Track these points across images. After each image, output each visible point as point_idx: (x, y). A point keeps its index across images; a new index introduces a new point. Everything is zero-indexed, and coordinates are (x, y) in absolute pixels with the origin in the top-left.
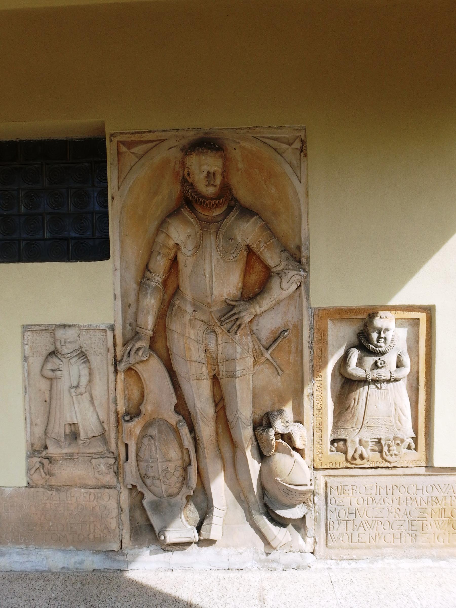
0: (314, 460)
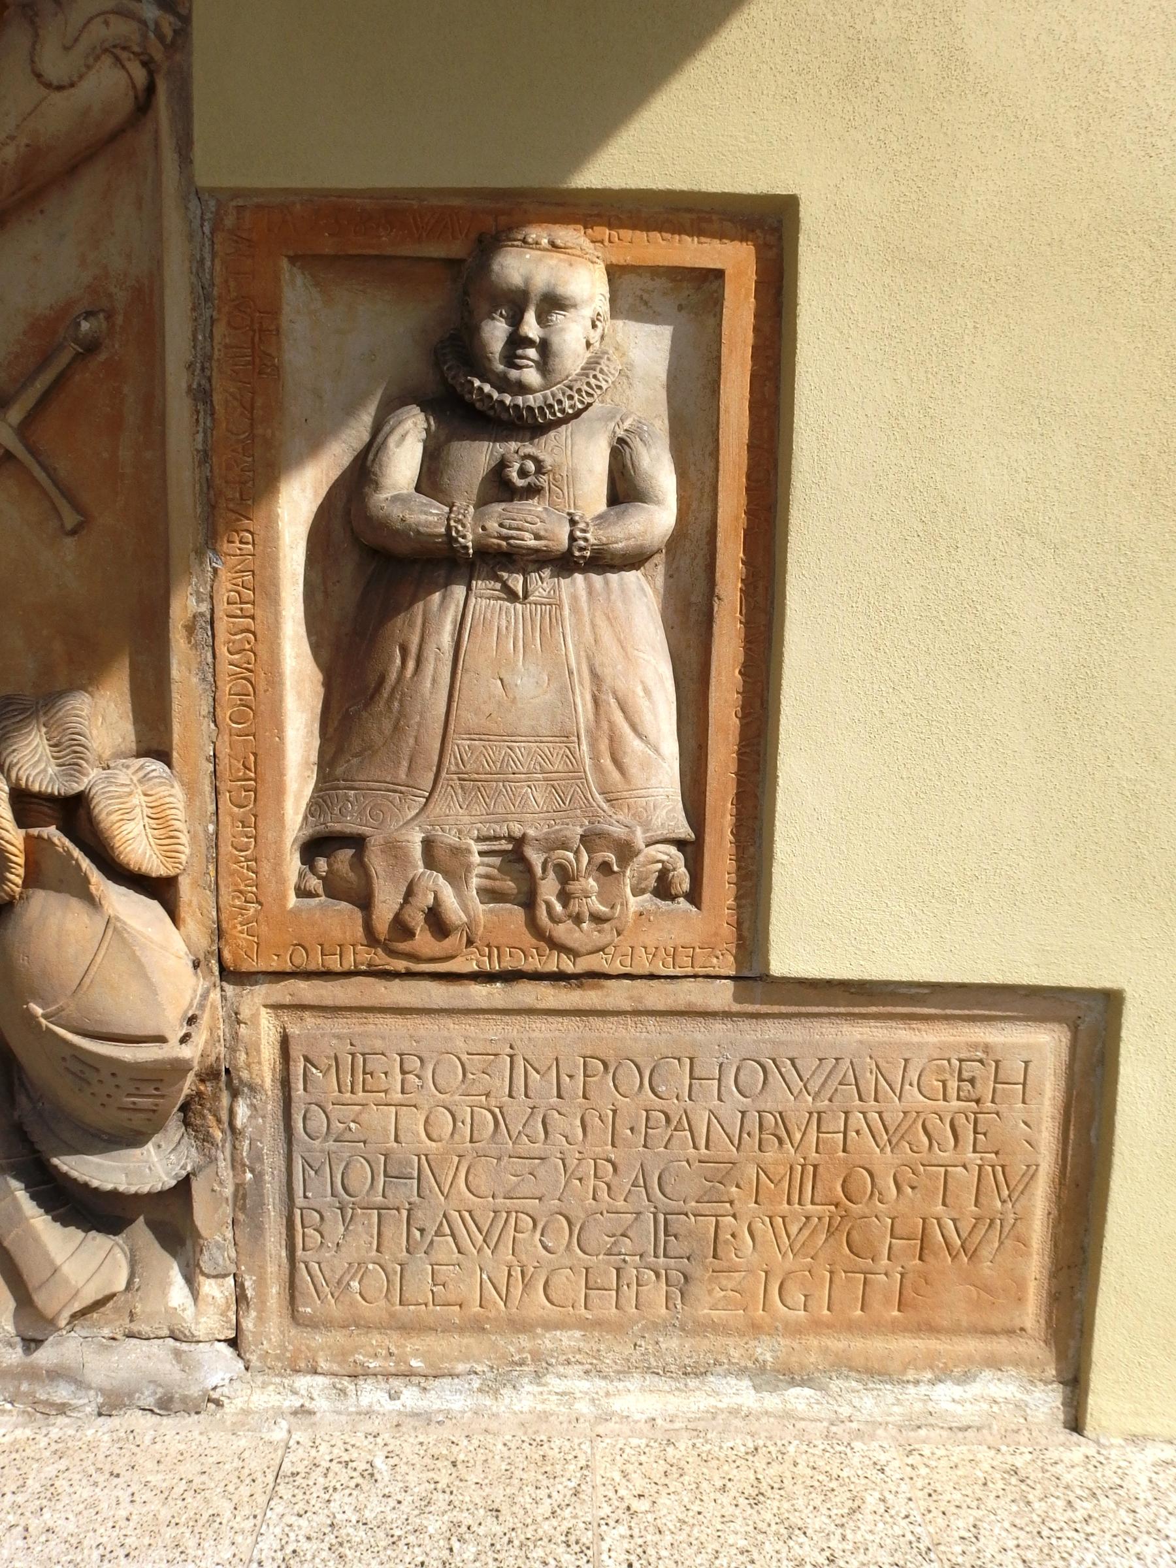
0: (220, 933)
